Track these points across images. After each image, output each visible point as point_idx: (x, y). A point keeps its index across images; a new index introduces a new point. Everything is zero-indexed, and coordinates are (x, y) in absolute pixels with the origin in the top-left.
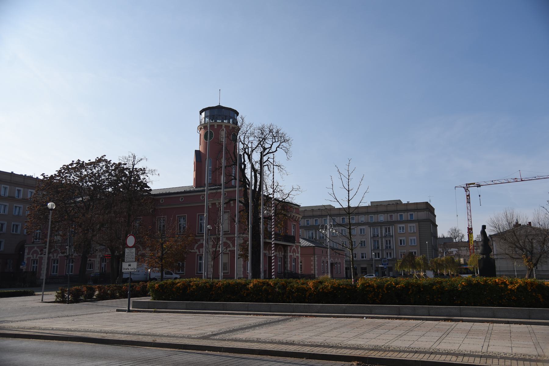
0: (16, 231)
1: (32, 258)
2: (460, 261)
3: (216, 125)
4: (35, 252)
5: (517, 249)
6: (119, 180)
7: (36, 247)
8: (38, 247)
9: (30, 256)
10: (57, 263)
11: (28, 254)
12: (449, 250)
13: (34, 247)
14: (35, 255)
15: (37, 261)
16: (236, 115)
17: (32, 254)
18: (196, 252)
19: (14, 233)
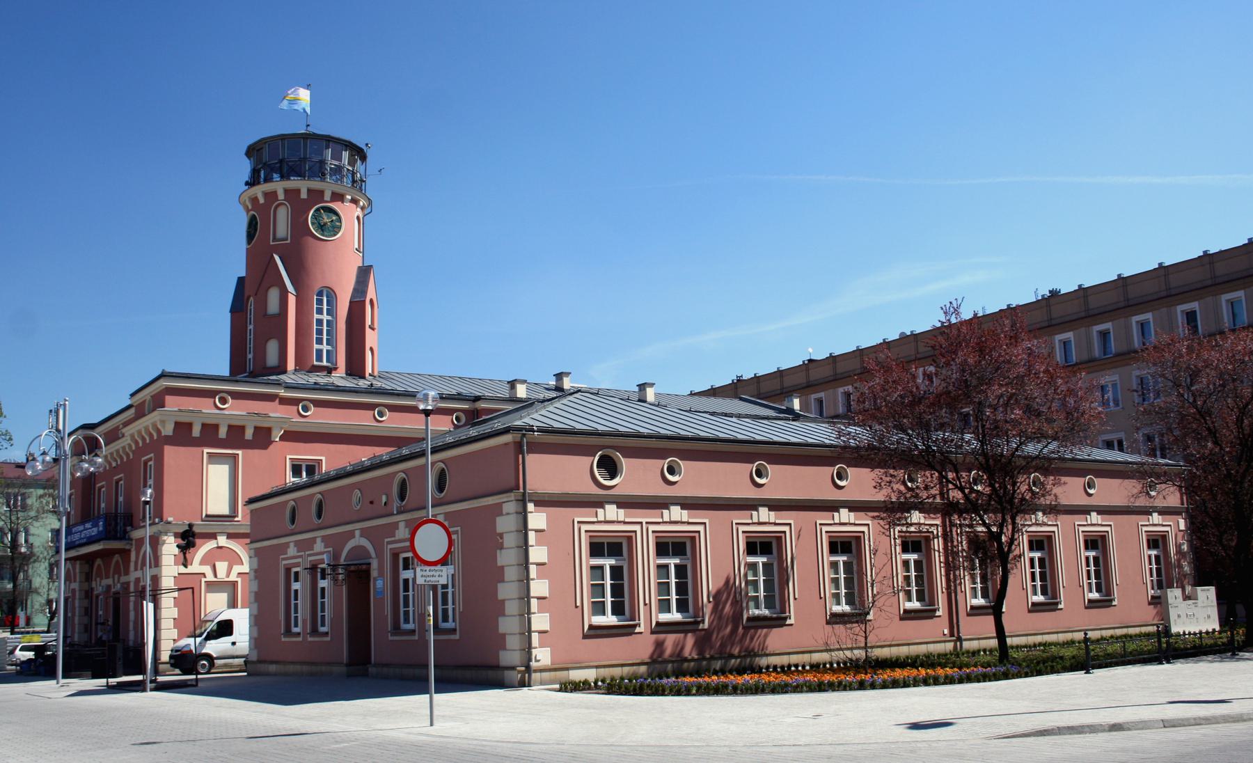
13: (351, 535)
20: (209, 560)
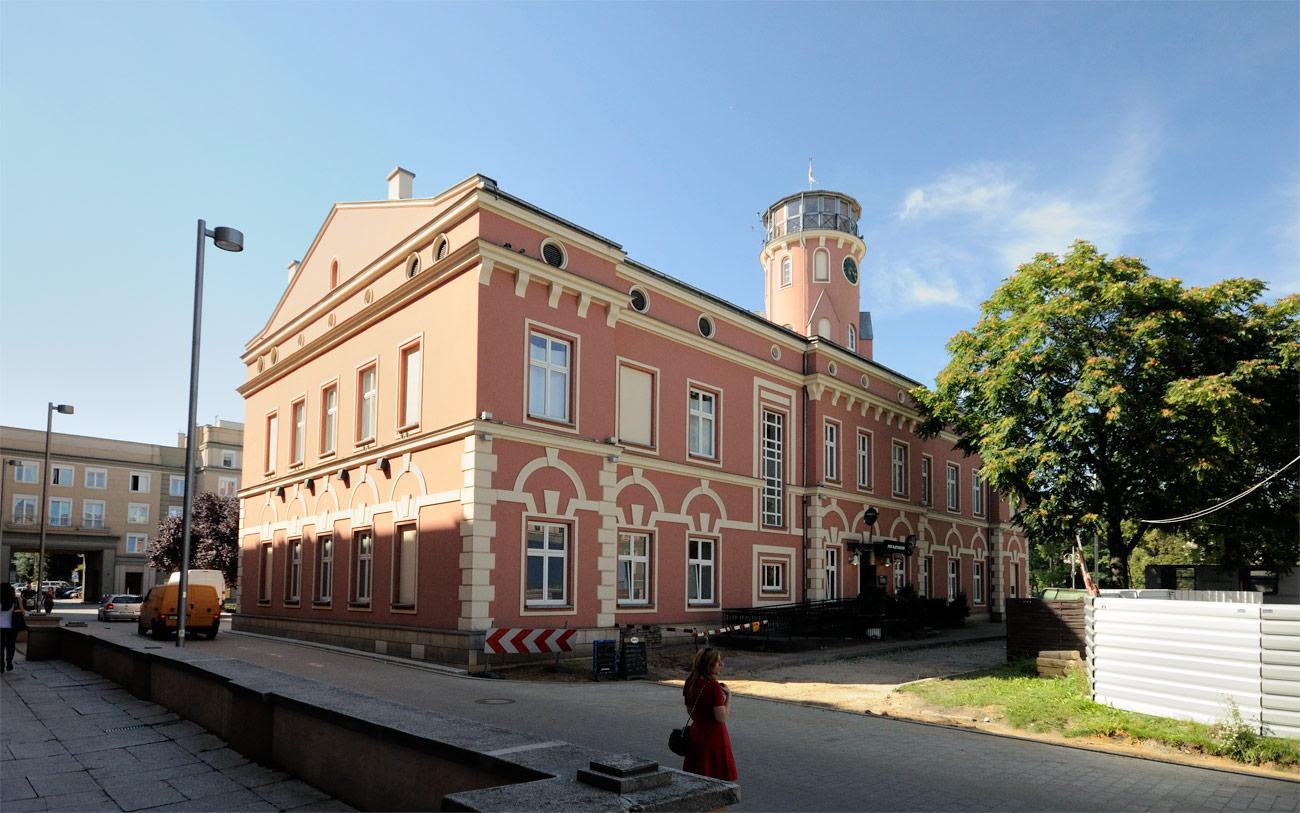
9: (517, 494)
13: (697, 482)
14: (552, 498)
20: (536, 486)
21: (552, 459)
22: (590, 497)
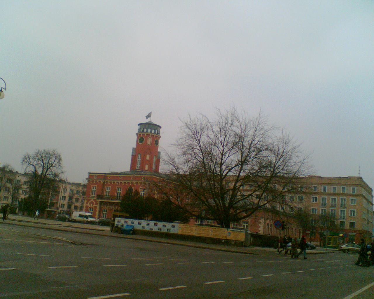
0: (315, 213)
1: (89, 207)
2: (370, 255)
3: (150, 135)
4: (92, 203)
5: (253, 158)
6: (38, 153)
7: (92, 200)
8: (94, 200)
9: (88, 205)
10: (106, 212)
11: (87, 203)
12: (280, 239)
13: (91, 199)
14: (91, 205)
15: (92, 209)
16: (159, 128)
17: (90, 204)
18: (88, 206)
19: (353, 216)
21: (92, 200)
22: (96, 204)
